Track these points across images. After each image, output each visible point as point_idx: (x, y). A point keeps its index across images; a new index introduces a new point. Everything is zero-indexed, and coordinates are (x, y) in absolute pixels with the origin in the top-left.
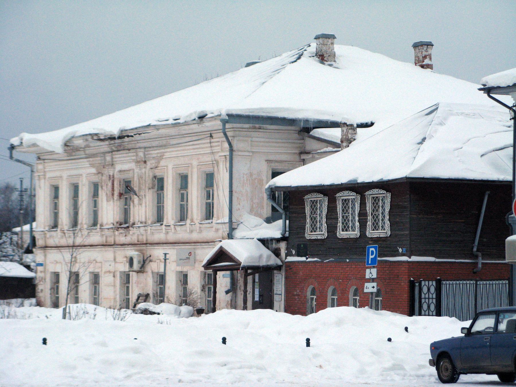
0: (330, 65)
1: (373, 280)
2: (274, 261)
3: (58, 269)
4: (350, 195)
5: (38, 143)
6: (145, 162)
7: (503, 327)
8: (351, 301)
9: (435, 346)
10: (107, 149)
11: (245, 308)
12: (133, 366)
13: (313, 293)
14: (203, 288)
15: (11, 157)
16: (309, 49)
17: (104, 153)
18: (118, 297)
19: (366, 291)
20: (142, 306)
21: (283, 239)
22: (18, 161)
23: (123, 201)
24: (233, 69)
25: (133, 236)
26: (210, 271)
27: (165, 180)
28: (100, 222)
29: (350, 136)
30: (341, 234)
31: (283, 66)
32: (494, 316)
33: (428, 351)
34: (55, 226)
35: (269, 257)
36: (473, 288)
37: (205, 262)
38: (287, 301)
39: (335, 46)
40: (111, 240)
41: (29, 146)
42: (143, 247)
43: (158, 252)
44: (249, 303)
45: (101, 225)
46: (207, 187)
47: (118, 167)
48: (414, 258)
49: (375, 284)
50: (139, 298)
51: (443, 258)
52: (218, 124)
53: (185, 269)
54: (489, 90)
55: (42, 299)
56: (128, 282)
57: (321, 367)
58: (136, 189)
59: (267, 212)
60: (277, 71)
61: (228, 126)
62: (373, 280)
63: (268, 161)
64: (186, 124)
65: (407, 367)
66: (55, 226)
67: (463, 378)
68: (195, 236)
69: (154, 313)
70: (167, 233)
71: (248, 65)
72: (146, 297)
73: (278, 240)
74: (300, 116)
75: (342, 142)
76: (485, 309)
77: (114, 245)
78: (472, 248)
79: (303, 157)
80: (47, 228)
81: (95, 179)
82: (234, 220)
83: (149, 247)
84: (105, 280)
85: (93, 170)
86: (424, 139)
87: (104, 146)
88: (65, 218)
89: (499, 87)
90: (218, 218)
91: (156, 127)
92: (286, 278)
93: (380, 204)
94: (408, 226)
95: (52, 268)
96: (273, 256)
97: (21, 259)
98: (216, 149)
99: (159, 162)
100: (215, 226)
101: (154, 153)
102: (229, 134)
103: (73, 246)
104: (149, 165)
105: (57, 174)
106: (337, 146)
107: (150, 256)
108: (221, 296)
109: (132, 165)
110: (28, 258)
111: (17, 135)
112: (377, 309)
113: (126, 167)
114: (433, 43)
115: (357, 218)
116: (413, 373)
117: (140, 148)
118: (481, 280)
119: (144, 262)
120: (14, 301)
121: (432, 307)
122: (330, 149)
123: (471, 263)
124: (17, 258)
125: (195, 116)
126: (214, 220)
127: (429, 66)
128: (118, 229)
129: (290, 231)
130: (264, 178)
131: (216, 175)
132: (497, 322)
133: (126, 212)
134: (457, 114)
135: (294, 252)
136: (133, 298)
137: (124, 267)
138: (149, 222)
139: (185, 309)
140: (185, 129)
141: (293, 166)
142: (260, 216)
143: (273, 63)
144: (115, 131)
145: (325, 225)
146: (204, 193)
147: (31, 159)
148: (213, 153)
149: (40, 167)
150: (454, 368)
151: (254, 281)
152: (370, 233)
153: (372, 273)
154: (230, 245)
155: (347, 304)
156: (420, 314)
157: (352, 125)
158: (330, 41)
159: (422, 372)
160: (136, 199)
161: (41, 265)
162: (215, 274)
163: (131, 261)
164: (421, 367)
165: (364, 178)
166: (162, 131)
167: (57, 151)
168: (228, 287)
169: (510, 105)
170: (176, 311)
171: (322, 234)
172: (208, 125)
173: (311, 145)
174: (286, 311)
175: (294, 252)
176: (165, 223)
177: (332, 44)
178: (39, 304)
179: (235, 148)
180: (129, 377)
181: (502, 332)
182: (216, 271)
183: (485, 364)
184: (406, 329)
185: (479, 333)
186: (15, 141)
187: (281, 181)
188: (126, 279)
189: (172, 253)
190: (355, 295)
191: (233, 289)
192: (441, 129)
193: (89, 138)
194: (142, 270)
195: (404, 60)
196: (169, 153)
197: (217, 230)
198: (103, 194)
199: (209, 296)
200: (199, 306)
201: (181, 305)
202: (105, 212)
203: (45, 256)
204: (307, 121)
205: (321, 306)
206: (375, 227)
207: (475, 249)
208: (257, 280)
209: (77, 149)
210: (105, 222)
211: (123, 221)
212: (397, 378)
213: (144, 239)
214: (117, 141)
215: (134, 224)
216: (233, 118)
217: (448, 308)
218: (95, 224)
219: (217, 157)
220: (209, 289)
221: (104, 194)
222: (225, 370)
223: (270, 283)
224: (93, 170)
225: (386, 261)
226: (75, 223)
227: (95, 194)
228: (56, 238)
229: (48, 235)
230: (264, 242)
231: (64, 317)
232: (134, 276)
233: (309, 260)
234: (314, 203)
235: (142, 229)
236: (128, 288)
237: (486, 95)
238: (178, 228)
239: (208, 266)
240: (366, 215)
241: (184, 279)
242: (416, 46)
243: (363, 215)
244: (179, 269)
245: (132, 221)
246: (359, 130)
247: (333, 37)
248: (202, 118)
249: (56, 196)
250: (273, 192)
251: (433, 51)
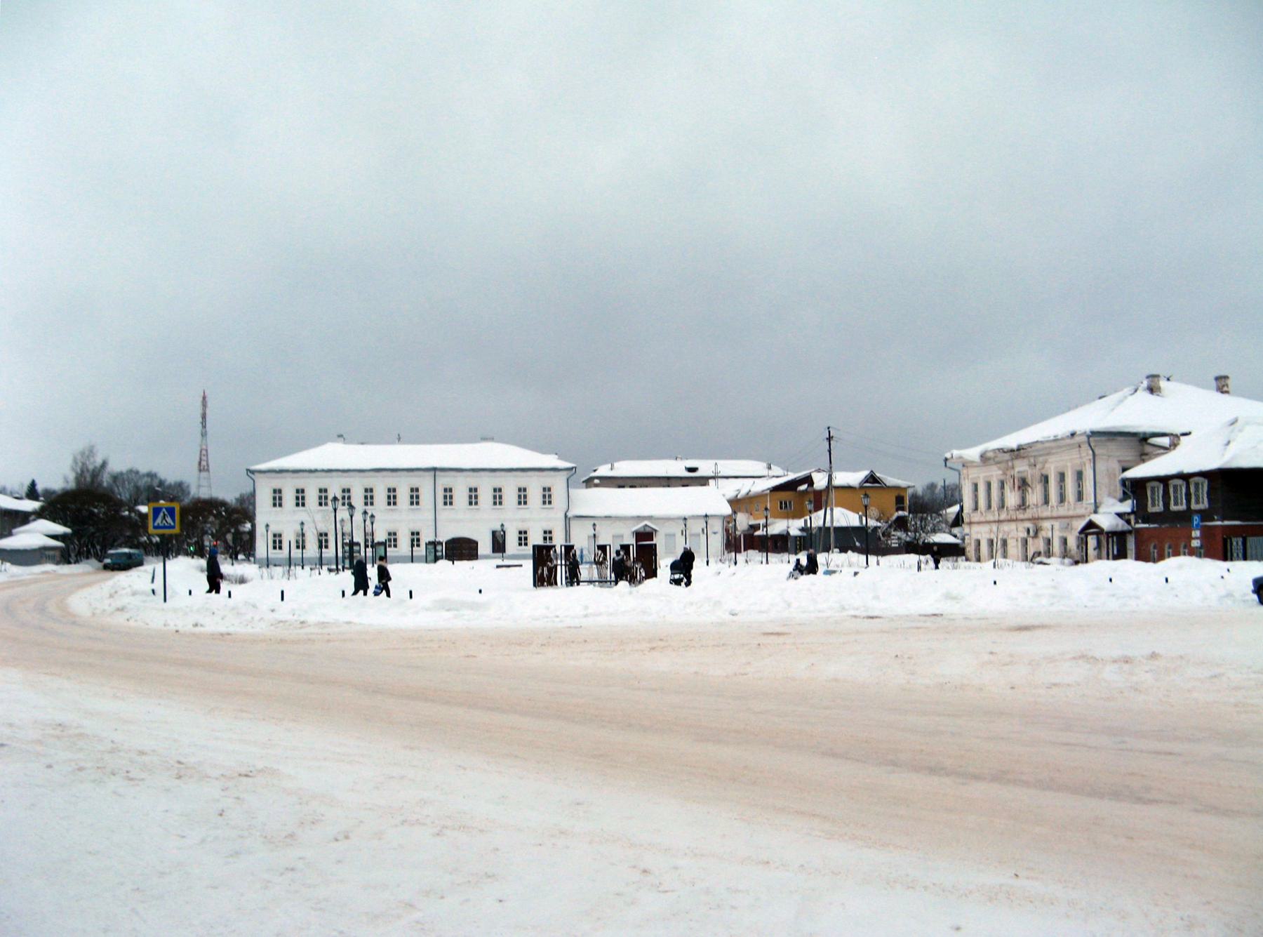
0: (1158, 395)
1: (1197, 538)
2: (1127, 527)
4: (1179, 482)
5: (964, 456)
6: (1035, 466)
11: (1108, 559)
13: (1155, 548)
14: (1078, 547)
16: (1142, 385)
17: (1007, 461)
18: (1020, 555)
20: (1038, 559)
21: (1133, 512)
22: (951, 468)
23: (1021, 491)
24: (1088, 401)
25: (1029, 514)
26: (1083, 536)
27: (1066, 474)
29: (1176, 442)
30: (1173, 508)
31: (1125, 397)
33: (1251, 584)
34: (976, 509)
35: (1123, 525)
38: (1136, 554)
41: (957, 458)
42: (1037, 521)
44: (1111, 556)
45: (1007, 508)
46: (1078, 479)
47: (1017, 469)
48: (1226, 523)
50: (1034, 554)
52: (1084, 438)
53: (1065, 535)
55: (970, 557)
58: (1030, 483)
59: (1119, 494)
61: (1091, 439)
62: (1197, 538)
63: (1119, 461)
64: (1062, 439)
66: (976, 509)
68: (1071, 513)
70: (1052, 511)
71: (1100, 398)
72: (1039, 554)
74: (1141, 430)
75: (1170, 446)
77: (1016, 520)
79: (1144, 457)
80: (971, 511)
81: (1002, 478)
83: (1040, 521)
84: (1011, 543)
85: (1000, 472)
87: (1007, 456)
91: (1042, 442)
92: (1135, 539)
93: (1200, 486)
95: (975, 536)
96: (1126, 524)
97: (951, 531)
100: (1084, 505)
101: (1041, 459)
102: (1092, 444)
104: (1038, 467)
105: (976, 475)
106: (1166, 449)
107: (303, 568)
108: (1091, 552)
110: (956, 530)
111: (949, 451)
117: (1031, 456)
120: (951, 558)
121: (1240, 555)
122: (1162, 451)
123: (1241, 526)
125: (1069, 434)
126: (1084, 501)
127: (1227, 392)
128: (1018, 510)
130: (1117, 473)
133: (1023, 499)
135: (1140, 521)
136: (1030, 554)
138: (1040, 505)
139: (1067, 561)
141: (1137, 464)
142: (1115, 497)
144: (1014, 446)
145: (1206, 499)
146: (1077, 484)
147: (960, 467)
149: (965, 471)
151: (1113, 541)
153: (1196, 533)
154: (1098, 519)
158: (1156, 379)
159: (1246, 598)
160: (1030, 490)
163: (1028, 531)
164: (1245, 595)
165: (1188, 469)
166: (1047, 445)
167: (976, 461)
171: (1159, 508)
172: (1077, 439)
173: (1148, 449)
175: (1140, 521)
178: (967, 560)
180: (1052, 604)
184: (1228, 570)
186: (948, 455)
188: (1025, 542)
189: (1057, 524)
191: (1099, 546)
193: (997, 451)
194: (1036, 535)
196: (1052, 459)
197: (1086, 509)
198: (1007, 488)
200: (1077, 559)
202: (1009, 499)
203: (970, 529)
204: (1145, 433)
206: (1197, 502)
208: (1115, 540)
209: (989, 459)
211: (1021, 504)
215: (1029, 506)
216: (1094, 434)
218: (1003, 507)
219: (1084, 460)
220: (1082, 548)
221: (1008, 487)
224: (1000, 472)
225: (1206, 526)
226: (989, 507)
227: (1002, 487)
228: (976, 517)
229: (972, 515)
230: (1120, 515)
231: (994, 567)
232: (1030, 541)
234: (1153, 489)
236: (1027, 548)
238: (1059, 508)
240: (1190, 494)
241: (1065, 541)
244: (1061, 535)
245: (1027, 504)
246: (1182, 438)
248: (1073, 435)
250: (1124, 482)
251: (1229, 382)
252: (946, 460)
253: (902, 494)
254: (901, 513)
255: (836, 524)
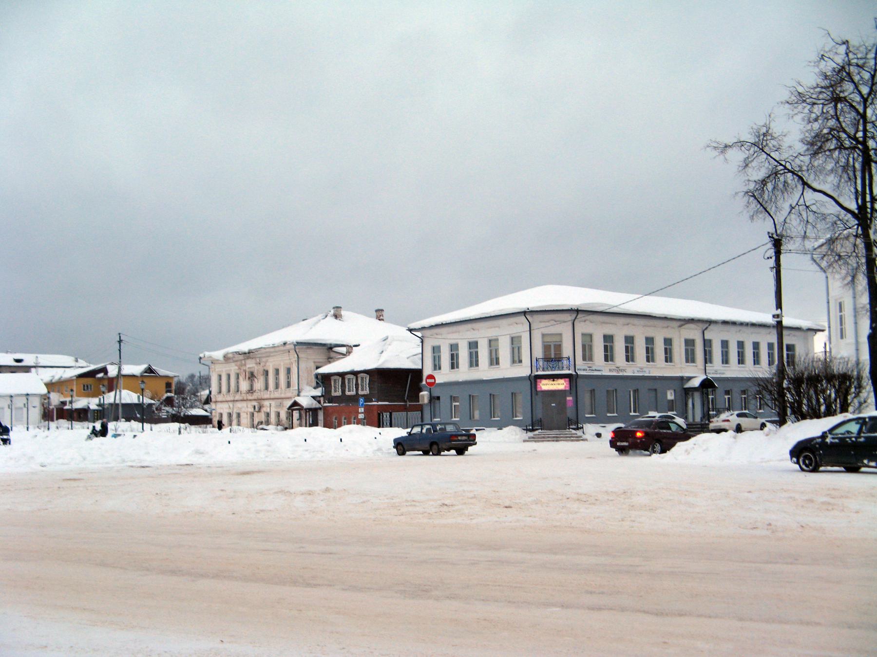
2: (318, 406)
3: (222, 411)
4: (337, 377)
7: (424, 431)
8: (353, 422)
9: (395, 440)
10: (243, 358)
11: (306, 426)
12: (268, 452)
14: (287, 418)
15: (200, 362)
16: (330, 313)
17: (241, 360)
18: (249, 424)
19: (359, 417)
20: (261, 426)
21: (322, 396)
22: (203, 364)
25: (255, 396)
26: (290, 411)
28: (240, 390)
29: (350, 350)
30: (347, 393)
31: (319, 321)
32: (420, 427)
34: (220, 392)
35: (316, 404)
36: (406, 415)
37: (288, 406)
39: (342, 311)
40: (245, 398)
42: (259, 401)
43: (267, 403)
45: (241, 392)
47: (248, 366)
48: (380, 403)
49: (363, 415)
50: (258, 423)
51: (392, 402)
52: (292, 347)
53: (278, 410)
54: (411, 330)
56: (253, 416)
57: (347, 450)
58: (256, 375)
59: (314, 384)
60: (317, 323)
61: (296, 347)
62: (362, 413)
63: (314, 362)
64: (278, 346)
65: (384, 449)
67: (408, 453)
68: (283, 396)
69: (266, 430)
70: (270, 394)
71: (304, 320)
72: (262, 423)
73: (320, 397)
74: (328, 342)
76: (417, 424)
78: (404, 398)
79: (329, 360)
81: (238, 371)
82: (300, 388)
84: (243, 415)
85: (237, 368)
86: (382, 352)
87: (241, 357)
88: (224, 388)
89: (415, 329)
90: (293, 387)
92: (324, 413)
93: (365, 380)
94: (377, 389)
95: (219, 411)
98: (291, 357)
99: (266, 363)
100: (291, 391)
101: (264, 360)
102: (297, 351)
103: (234, 401)
104: (262, 364)
105: (220, 370)
109: (254, 365)
112: (364, 425)
113: (251, 366)
114: (384, 309)
115: (354, 386)
116: (386, 452)
118: (409, 411)
119: (260, 408)
120: (202, 426)
121: (388, 424)
122: (342, 356)
124: (201, 407)
126: (291, 388)
127: (383, 320)
128: (248, 393)
129: (114, 406)
130: (313, 369)
131: (292, 369)
132: (422, 429)
133: (252, 386)
134: (397, 340)
136: (256, 423)
137: (252, 410)
138: (262, 390)
139: (280, 427)
140: (277, 349)
141: (326, 364)
142: (312, 386)
143: (315, 319)
144: (246, 350)
145: (340, 390)
146: (287, 377)
147: (209, 363)
148: (290, 359)
149: (213, 367)
150: (404, 449)
151: (309, 414)
152: (360, 392)
153: (361, 410)
155: (350, 424)
156: (383, 427)
157: (351, 346)
158: (339, 309)
159: (390, 451)
161: (214, 410)
162: (292, 412)
163: (254, 407)
165: (357, 369)
166: (267, 350)
168: (298, 417)
169: (420, 336)
170: (276, 428)
171: (339, 393)
172: (287, 347)
174: (324, 426)
175: (327, 402)
176: (269, 390)
177: (340, 310)
178: (214, 427)
179: (300, 356)
180: (267, 457)
181: (424, 433)
182: (292, 411)
183: (417, 447)
184: (380, 433)
185: (414, 434)
186: (202, 355)
187: (321, 371)
188: (252, 415)
189: (273, 403)
190: (354, 419)
191: (300, 418)
192: (390, 347)
194: (259, 411)
195: (370, 317)
196: (271, 359)
198: (241, 378)
199: (290, 422)
200: (286, 426)
201: (277, 425)
203: (216, 405)
204: (331, 344)
205: (340, 425)
206: (362, 390)
207: (406, 398)
209: (229, 359)
210: (242, 390)
212: (379, 454)
213: (260, 397)
214: (247, 355)
216: (299, 343)
217: (395, 424)
218: (238, 391)
221: (242, 379)
222: (307, 453)
223: (317, 415)
230: (314, 397)
231: (231, 432)
232: (256, 414)
233: (334, 405)
234: (335, 381)
235: (259, 393)
236: (253, 419)
237: (409, 332)
239: (289, 409)
241: (278, 414)
242: (376, 311)
243: (357, 384)
244: (276, 410)
246: (354, 348)
247: (341, 307)
248: (285, 344)
249: (220, 379)
250: (317, 376)
251: (384, 313)
252: (200, 358)
253: (170, 381)
254: (169, 394)
255: (123, 402)
